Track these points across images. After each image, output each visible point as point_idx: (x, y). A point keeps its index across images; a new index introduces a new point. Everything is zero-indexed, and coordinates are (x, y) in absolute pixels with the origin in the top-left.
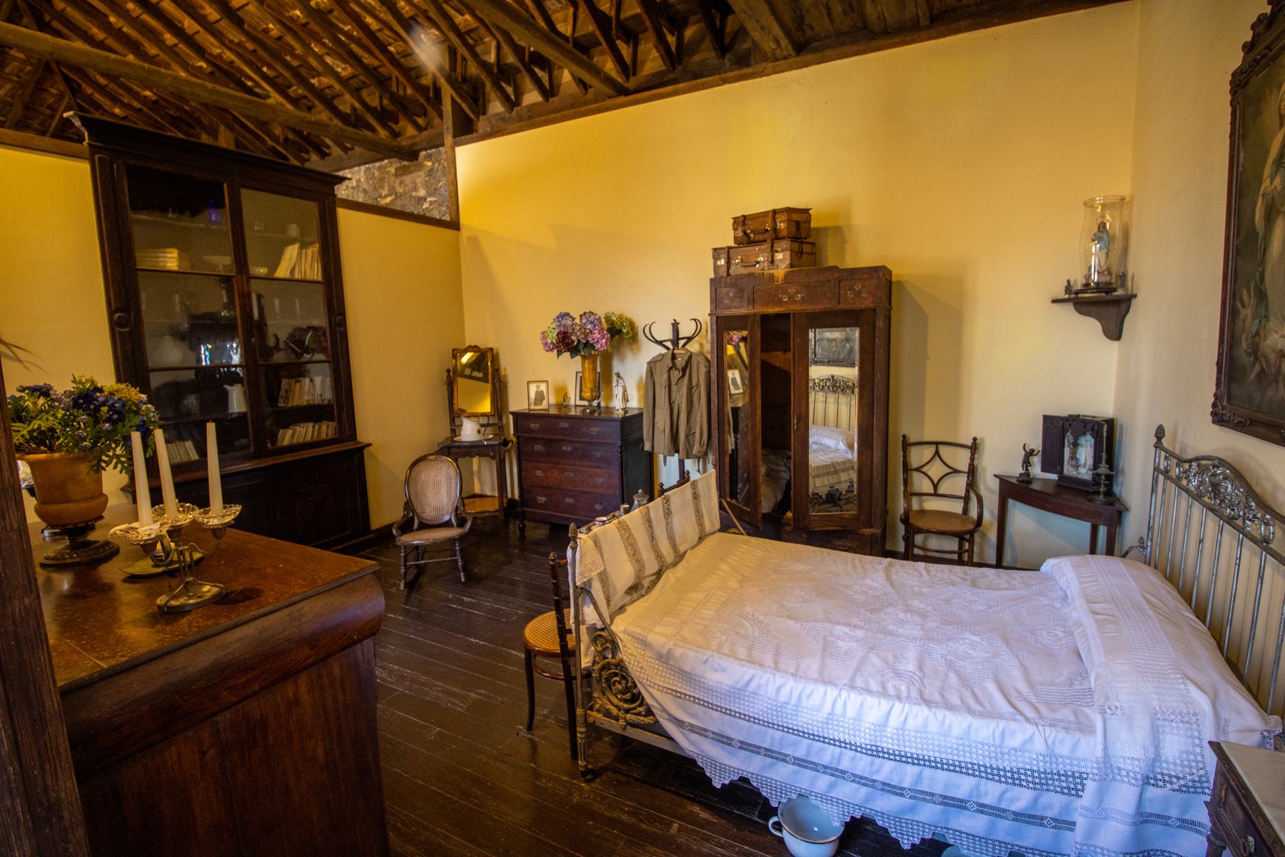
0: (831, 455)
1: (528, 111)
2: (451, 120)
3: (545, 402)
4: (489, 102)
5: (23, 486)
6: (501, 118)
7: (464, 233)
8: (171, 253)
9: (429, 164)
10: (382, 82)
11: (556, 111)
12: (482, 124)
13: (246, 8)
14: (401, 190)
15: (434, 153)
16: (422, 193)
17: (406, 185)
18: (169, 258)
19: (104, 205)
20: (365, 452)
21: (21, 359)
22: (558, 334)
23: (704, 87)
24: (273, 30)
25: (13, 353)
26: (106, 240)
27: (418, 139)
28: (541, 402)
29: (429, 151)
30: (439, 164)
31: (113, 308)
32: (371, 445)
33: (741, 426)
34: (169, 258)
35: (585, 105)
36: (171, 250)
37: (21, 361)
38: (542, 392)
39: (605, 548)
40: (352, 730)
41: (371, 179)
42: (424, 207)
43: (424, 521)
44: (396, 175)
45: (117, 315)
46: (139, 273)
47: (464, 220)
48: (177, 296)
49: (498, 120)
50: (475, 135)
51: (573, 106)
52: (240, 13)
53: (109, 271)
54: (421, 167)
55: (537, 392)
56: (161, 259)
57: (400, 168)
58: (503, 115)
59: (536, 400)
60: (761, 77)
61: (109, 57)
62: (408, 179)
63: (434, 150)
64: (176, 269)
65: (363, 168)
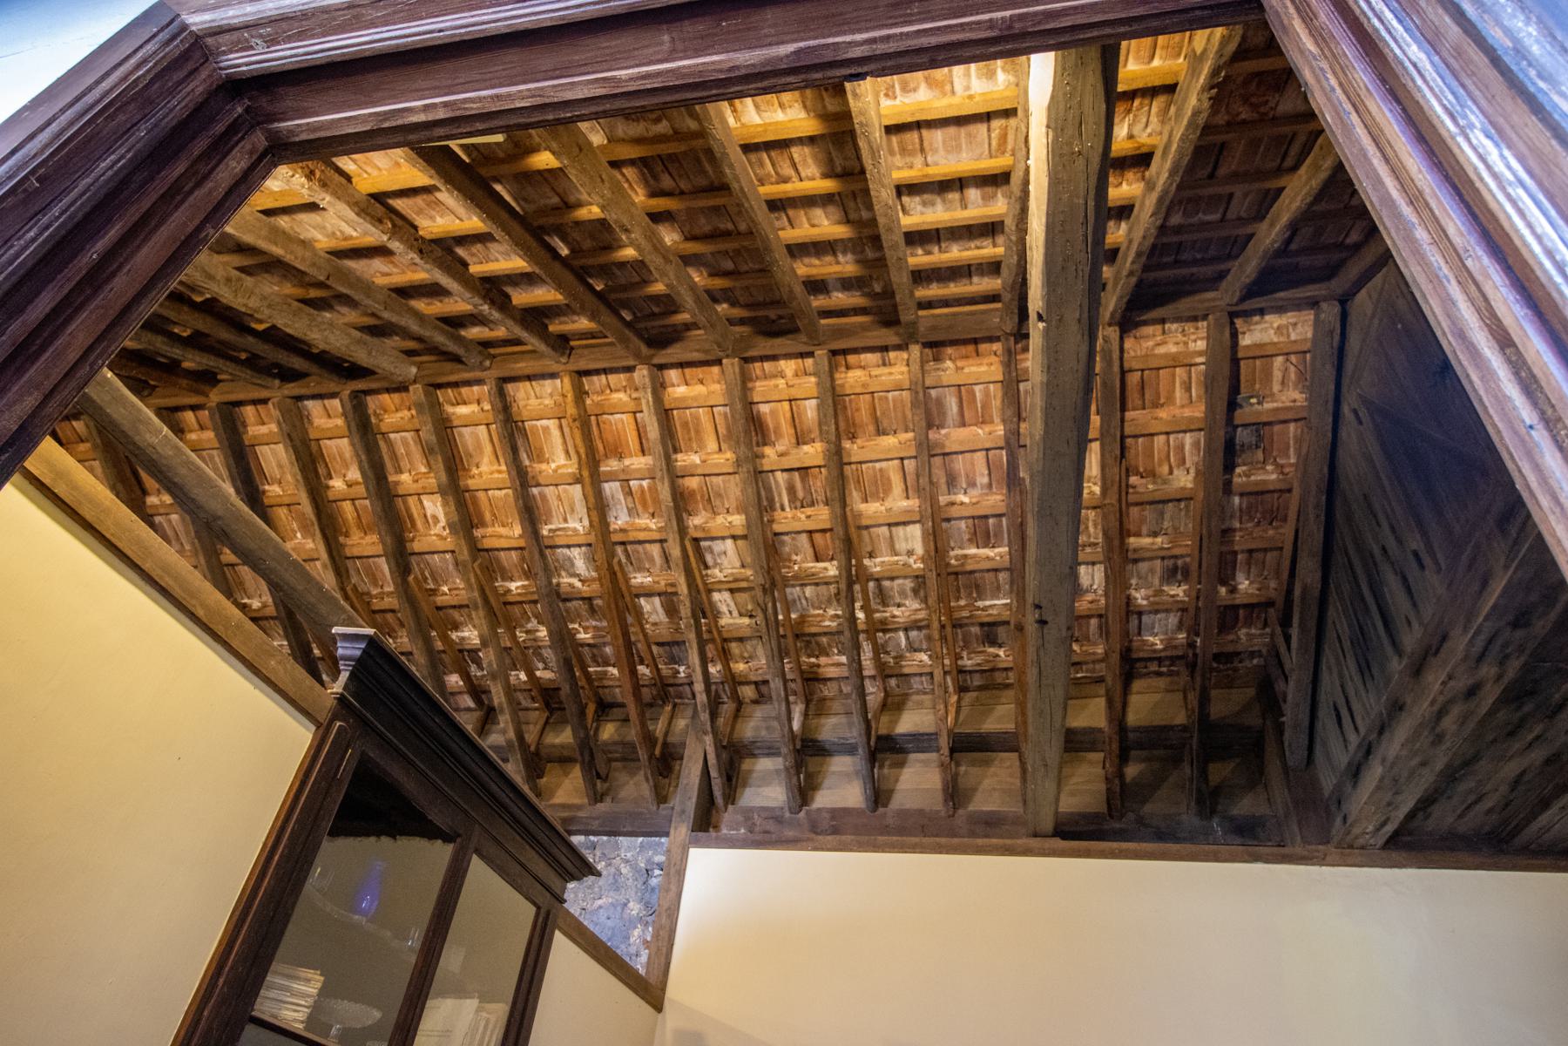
1: (833, 818)
2: (694, 800)
6: (774, 816)
7: (671, 1019)
10: (1269, 700)
12: (729, 819)
15: (603, 843)
23: (1087, 854)
27: (581, 814)
33: (769, 353)
35: (947, 836)
39: (894, 574)
40: (947, 662)
50: (712, 833)
51: (924, 830)
58: (778, 813)
60: (1322, 865)
63: (605, 838)
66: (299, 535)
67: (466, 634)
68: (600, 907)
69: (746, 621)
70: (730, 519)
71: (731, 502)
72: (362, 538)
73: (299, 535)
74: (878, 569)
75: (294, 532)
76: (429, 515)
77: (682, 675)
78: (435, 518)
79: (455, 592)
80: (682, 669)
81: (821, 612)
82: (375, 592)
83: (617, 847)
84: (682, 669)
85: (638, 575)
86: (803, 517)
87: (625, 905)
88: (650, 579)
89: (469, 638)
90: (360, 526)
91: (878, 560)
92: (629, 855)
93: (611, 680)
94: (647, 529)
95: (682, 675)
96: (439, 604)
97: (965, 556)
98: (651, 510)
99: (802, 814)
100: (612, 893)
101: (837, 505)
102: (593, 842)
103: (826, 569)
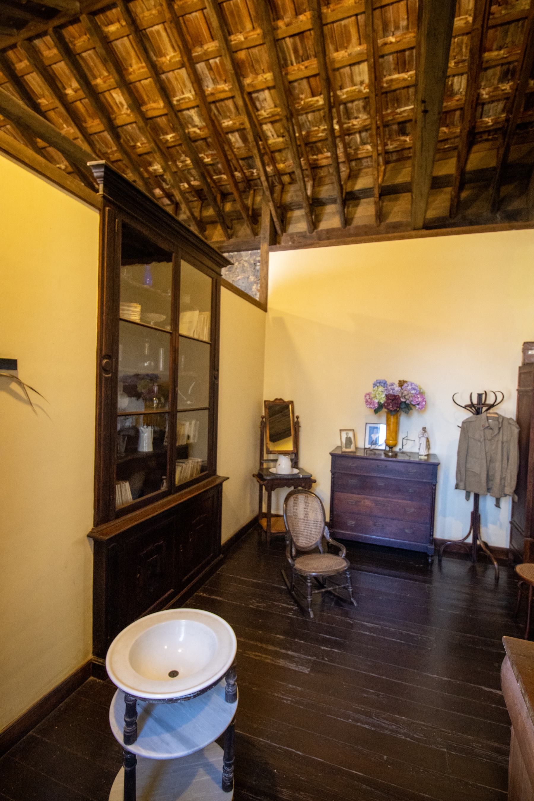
1: (327, 233)
2: (268, 232)
3: (353, 446)
4: (289, 224)
5: (217, 572)
6: (302, 235)
7: (271, 314)
8: (136, 307)
11: (350, 236)
12: (284, 239)
13: (125, 127)
15: (236, 255)
18: (133, 311)
19: (108, 254)
20: (225, 484)
21: (32, 402)
22: (398, 396)
24: (139, 147)
25: (26, 394)
26: (105, 289)
27: (225, 244)
28: (350, 446)
29: (231, 254)
30: (239, 263)
31: (104, 353)
32: (227, 478)
34: (133, 311)
36: (135, 305)
37: (31, 404)
38: (350, 438)
43: (299, 549)
45: (105, 361)
46: (121, 323)
47: (270, 305)
49: (299, 237)
50: (278, 245)
52: (119, 130)
53: (104, 318)
55: (347, 438)
56: (126, 312)
59: (346, 444)
63: (236, 253)
64: (138, 321)
68: (239, 279)
72: (92, 122)
73: (65, 126)
74: (345, 96)
78: (121, 103)
79: (144, 145)
82: (109, 151)
83: (241, 256)
85: (225, 121)
86: (303, 68)
91: (345, 90)
94: (224, 91)
97: (392, 80)
98: (224, 78)
99: (314, 233)
100: (243, 274)
103: (318, 101)
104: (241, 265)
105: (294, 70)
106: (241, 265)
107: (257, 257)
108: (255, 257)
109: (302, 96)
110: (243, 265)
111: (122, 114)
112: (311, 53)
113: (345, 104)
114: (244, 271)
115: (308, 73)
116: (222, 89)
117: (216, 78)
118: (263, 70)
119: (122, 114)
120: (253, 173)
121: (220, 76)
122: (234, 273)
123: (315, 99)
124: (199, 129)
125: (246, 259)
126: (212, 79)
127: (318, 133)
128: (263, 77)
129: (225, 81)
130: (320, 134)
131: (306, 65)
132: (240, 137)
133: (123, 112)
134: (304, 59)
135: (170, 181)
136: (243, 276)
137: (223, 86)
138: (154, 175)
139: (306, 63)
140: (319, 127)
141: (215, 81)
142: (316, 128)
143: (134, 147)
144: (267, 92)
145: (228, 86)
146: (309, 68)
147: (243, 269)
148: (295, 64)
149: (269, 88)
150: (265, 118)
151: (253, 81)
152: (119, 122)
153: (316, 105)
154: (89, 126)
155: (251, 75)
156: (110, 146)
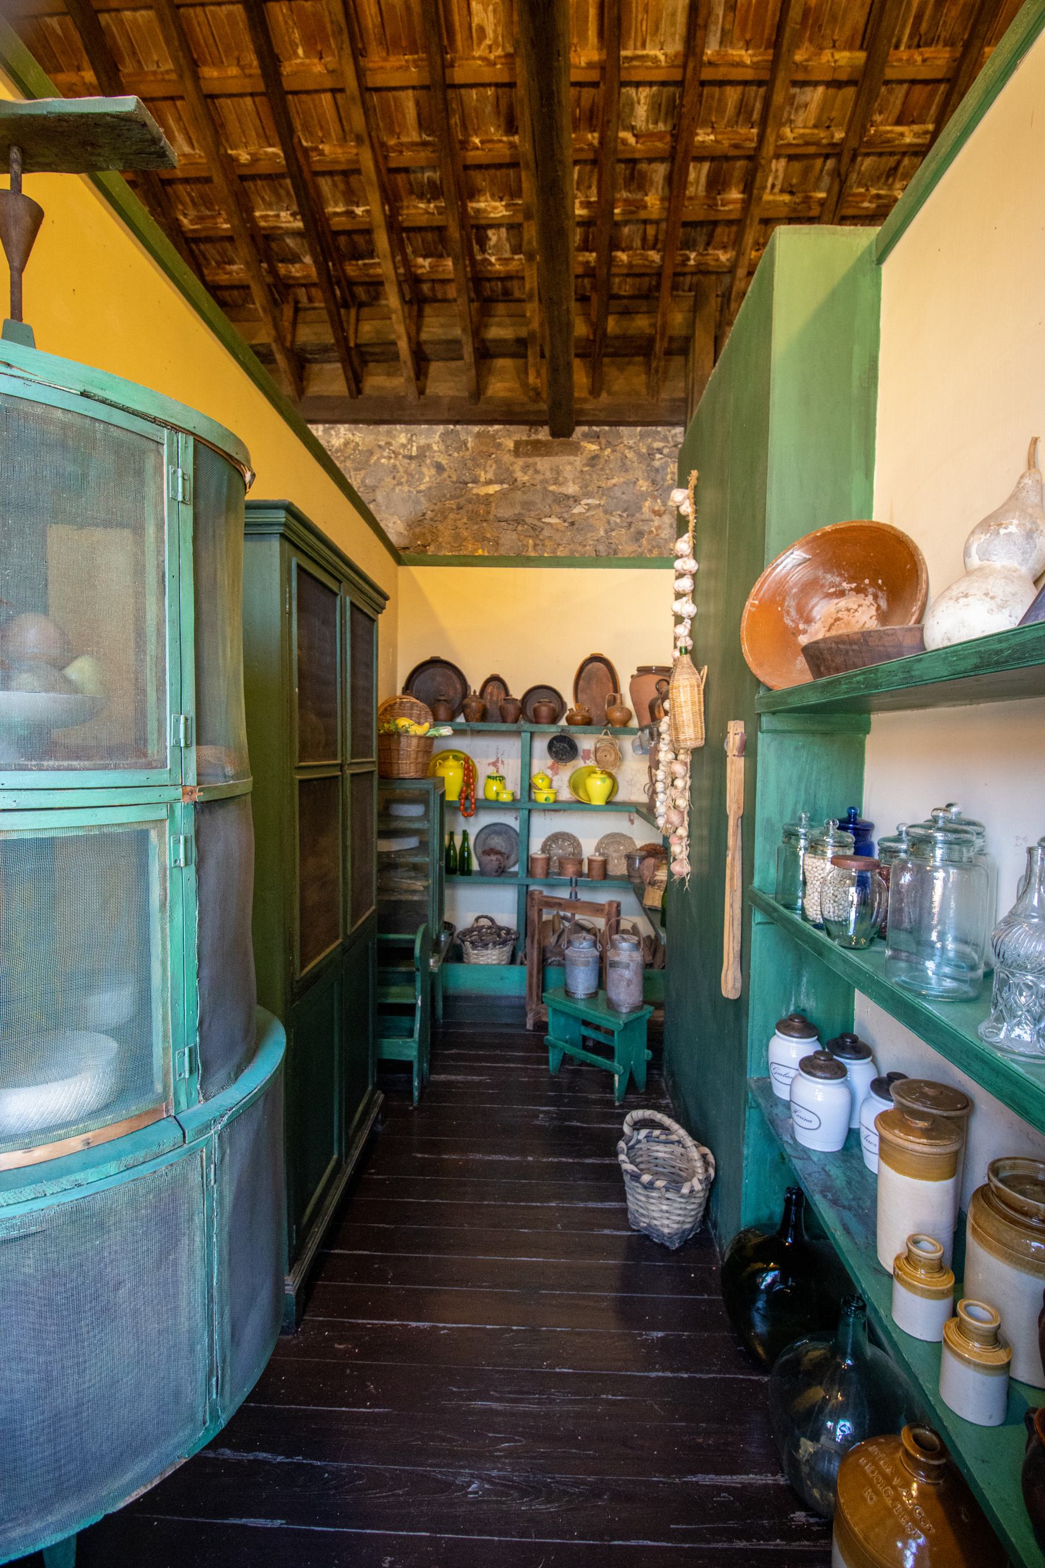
0: (756, 1045)
9: (594, 447)
13: (463, 91)
14: (526, 478)
15: (606, 433)
16: (571, 489)
17: (537, 472)
29: (595, 428)
30: (613, 451)
41: (458, 449)
42: (575, 511)
44: (517, 452)
48: (815, 1490)
54: (576, 449)
57: (527, 443)
61: (493, 1541)
62: (543, 464)
63: (607, 428)
65: (440, 429)
66: (300, 52)
67: (482, 205)
68: (615, 485)
69: (786, 198)
70: (837, 56)
71: (841, 34)
72: (385, 60)
73: (300, 52)
75: (294, 46)
76: (474, 26)
77: (692, 262)
78: (481, 30)
79: (490, 146)
80: (693, 255)
81: (862, 190)
82: (392, 142)
83: (619, 436)
84: (693, 255)
86: (919, 59)
87: (635, 483)
88: (712, 137)
89: (485, 211)
90: (382, 41)
92: (631, 442)
93: (619, 266)
94: (740, 64)
95: (692, 262)
96: (469, 162)
98: (748, 36)
100: (623, 474)
101: (959, 49)
102: (596, 432)
103: (902, 135)
104: (619, 455)
105: (900, 60)
106: (619, 455)
107: (655, 440)
108: (650, 440)
109: (878, 118)
110: (623, 454)
111: (474, 58)
112: (943, 34)
113: (632, 162)
114: (624, 468)
115: (925, 74)
116: (737, 59)
117: (731, 31)
118: (834, 42)
119: (474, 58)
120: (688, 259)
121: (743, 30)
122: (602, 469)
123: (899, 129)
124: (635, 136)
125: (631, 442)
126: (723, 29)
127: (863, 201)
128: (833, 56)
129: (748, 45)
130: (866, 204)
131: (926, 55)
132: (708, 175)
133: (477, 54)
134: (921, 44)
135: (530, 242)
136: (622, 480)
137: (743, 52)
138: (473, 222)
139: (928, 52)
140: (867, 190)
141: (725, 39)
142: (862, 190)
143: (464, 144)
144: (248, 100)
145: (751, 56)
146: (928, 63)
147: (624, 464)
148: (902, 48)
149: (252, 95)
150: (790, 145)
151: (807, 60)
152: (459, 75)
153: (897, 142)
154: (371, 65)
155: (807, 44)
156: (594, 122)
